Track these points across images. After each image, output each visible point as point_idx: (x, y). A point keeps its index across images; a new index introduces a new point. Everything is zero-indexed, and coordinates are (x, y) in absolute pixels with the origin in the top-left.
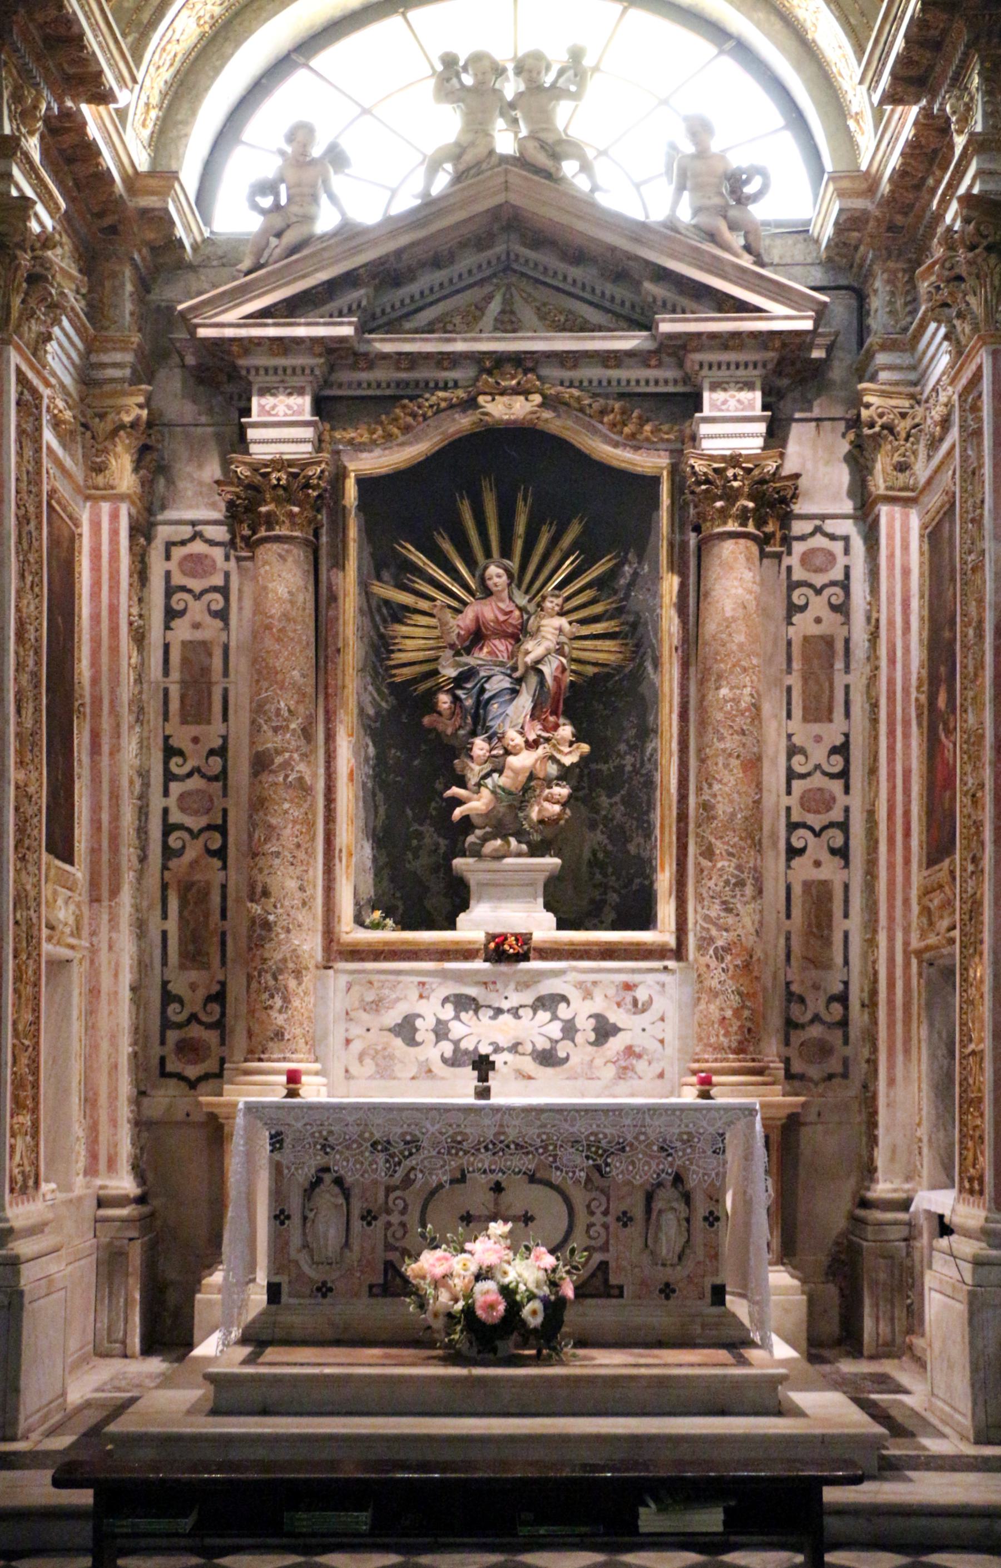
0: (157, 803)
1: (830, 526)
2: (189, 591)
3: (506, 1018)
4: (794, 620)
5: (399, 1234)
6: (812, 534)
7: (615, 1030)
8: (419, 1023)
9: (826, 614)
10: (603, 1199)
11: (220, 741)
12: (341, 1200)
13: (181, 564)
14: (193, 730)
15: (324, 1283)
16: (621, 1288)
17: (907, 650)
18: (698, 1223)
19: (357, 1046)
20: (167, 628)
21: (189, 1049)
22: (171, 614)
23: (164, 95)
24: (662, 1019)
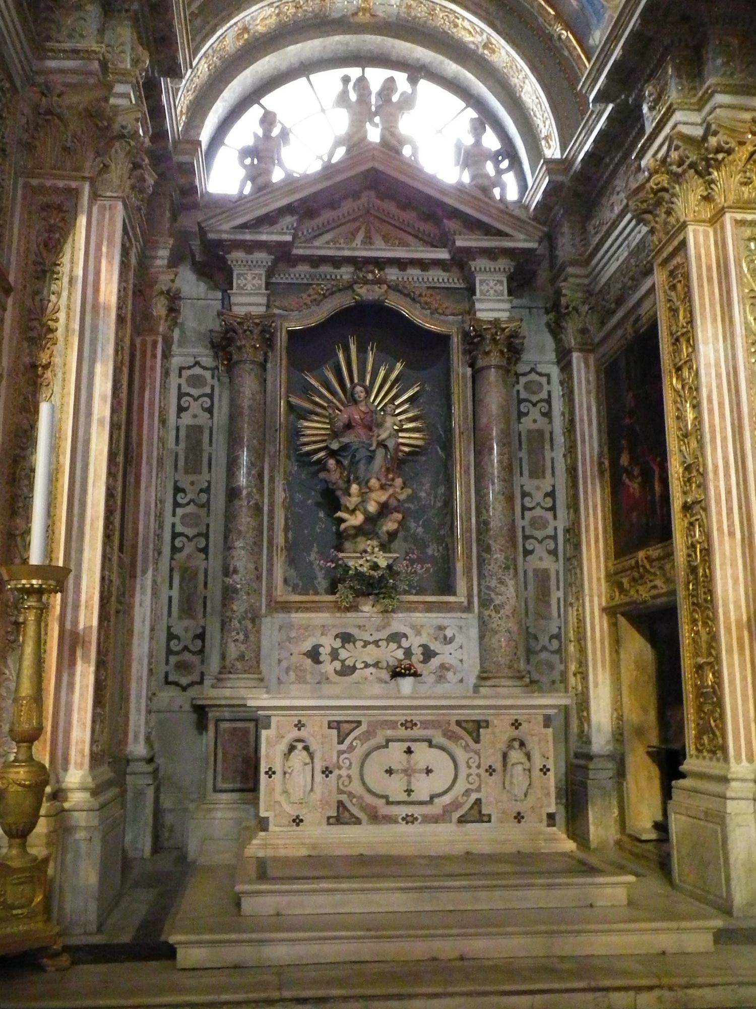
0: (168, 520)
1: (540, 368)
2: (191, 396)
3: (371, 647)
4: (522, 420)
5: (346, 783)
6: (530, 372)
7: (435, 654)
8: (321, 650)
9: (538, 417)
10: (477, 758)
11: (206, 484)
12: (308, 760)
13: (187, 380)
14: (192, 478)
15: (298, 817)
16: (489, 816)
17: (591, 436)
18: (536, 773)
19: (284, 664)
20: (179, 417)
21: (182, 667)
22: (181, 409)
23: (188, 109)
24: (461, 647)
